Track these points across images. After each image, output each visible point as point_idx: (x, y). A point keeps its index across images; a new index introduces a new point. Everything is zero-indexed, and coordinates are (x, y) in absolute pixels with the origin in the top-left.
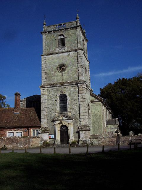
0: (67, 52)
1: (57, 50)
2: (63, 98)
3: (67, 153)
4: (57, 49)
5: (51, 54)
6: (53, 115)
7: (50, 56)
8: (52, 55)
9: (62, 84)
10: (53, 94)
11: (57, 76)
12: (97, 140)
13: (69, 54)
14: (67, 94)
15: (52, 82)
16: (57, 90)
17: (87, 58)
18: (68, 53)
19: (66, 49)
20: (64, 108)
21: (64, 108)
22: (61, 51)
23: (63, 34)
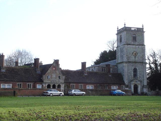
0: (137, 45)
1: (132, 43)
2: (135, 70)
3: (138, 90)
4: (132, 42)
5: (130, 44)
6: (130, 78)
7: (129, 46)
8: (119, 40)
9: (135, 62)
10: (131, 67)
11: (132, 58)
12: (150, 93)
13: (139, 47)
14: (137, 68)
15: (130, 61)
16: (133, 66)
17: (8, 80)
18: (138, 46)
19: (137, 43)
20: (135, 75)
21: (135, 75)
22: (134, 44)
23: (136, 34)
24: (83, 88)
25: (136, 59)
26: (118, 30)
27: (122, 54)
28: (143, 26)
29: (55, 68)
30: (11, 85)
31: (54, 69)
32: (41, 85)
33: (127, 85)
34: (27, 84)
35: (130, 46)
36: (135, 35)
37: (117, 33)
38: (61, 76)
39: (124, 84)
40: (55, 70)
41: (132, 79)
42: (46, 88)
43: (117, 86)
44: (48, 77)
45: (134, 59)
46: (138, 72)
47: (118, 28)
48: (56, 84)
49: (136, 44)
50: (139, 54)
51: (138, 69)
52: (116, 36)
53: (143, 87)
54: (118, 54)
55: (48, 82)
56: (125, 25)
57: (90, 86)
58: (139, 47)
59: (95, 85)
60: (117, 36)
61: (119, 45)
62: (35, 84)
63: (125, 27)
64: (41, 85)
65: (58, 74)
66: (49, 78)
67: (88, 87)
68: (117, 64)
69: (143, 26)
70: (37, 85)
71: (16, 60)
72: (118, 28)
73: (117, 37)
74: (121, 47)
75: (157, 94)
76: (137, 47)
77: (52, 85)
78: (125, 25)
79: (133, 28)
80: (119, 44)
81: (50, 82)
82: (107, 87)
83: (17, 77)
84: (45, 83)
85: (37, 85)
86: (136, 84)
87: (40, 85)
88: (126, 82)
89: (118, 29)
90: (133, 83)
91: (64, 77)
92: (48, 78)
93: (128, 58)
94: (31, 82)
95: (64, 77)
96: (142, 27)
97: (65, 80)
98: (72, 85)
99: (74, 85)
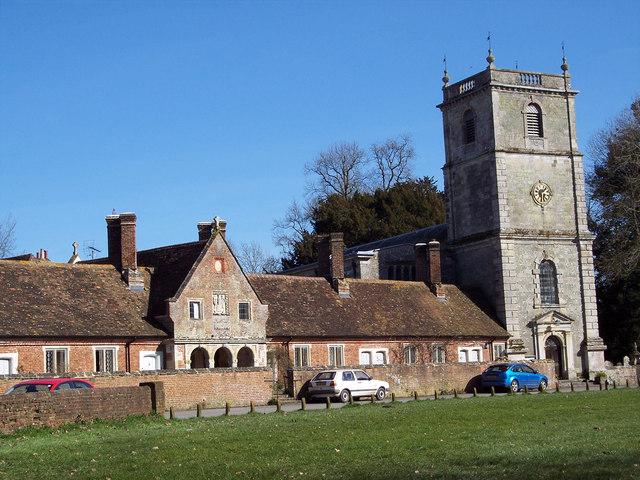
1: (529, 145)
7: (515, 156)
13: (555, 161)
14: (556, 262)
15: (522, 226)
18: (553, 158)
22: (535, 148)
24: (388, 360)
25: (549, 216)
26: (445, 89)
27: (482, 196)
29: (222, 260)
30: (15, 356)
31: (218, 265)
33: (517, 340)
34: (44, 349)
38: (252, 300)
40: (223, 270)
43: (480, 348)
44: (192, 310)
45: (537, 217)
48: (228, 346)
50: (557, 195)
52: (439, 113)
54: (455, 199)
55: (193, 335)
57: (374, 351)
58: (555, 161)
59: (394, 344)
61: (460, 155)
66: (196, 316)
68: (455, 243)
71: (609, 141)
72: (445, 80)
74: (472, 163)
79: (464, 82)
80: (459, 150)
81: (202, 334)
82: (440, 355)
83: (38, 311)
85: (142, 353)
89: (448, 85)
91: (264, 308)
92: (192, 315)
93: (516, 216)
94: (111, 339)
95: (264, 308)
97: (271, 323)
98: (297, 349)
99: (110, 353)
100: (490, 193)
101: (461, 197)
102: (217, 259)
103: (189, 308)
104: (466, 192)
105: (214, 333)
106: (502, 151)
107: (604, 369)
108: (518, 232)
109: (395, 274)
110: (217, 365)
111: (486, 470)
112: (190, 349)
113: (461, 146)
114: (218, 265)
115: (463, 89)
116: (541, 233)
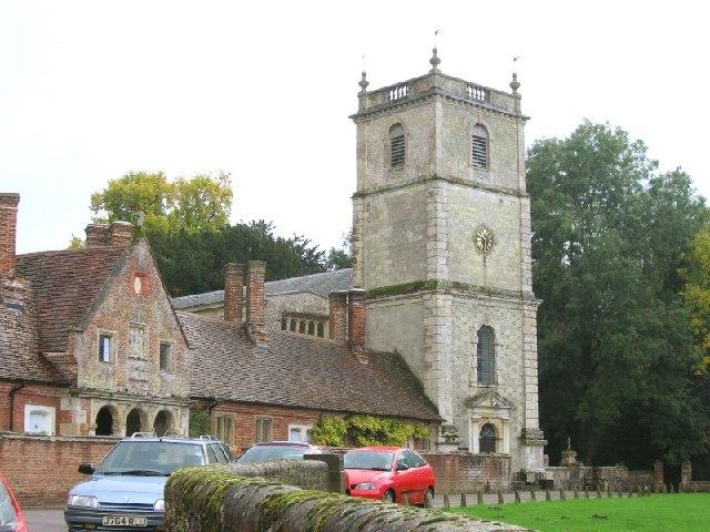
1: (471, 175)
7: (456, 188)
13: (501, 201)
14: (497, 328)
25: (490, 271)
26: (361, 96)
28: (515, 86)
29: (142, 276)
32: (51, 411)
35: (482, 198)
36: (483, 127)
37: (355, 110)
39: (435, 421)
40: (143, 292)
41: (473, 393)
42: (93, 433)
46: (498, 349)
47: (364, 84)
48: (145, 408)
49: (486, 182)
51: (498, 335)
52: (353, 127)
53: (523, 439)
56: (435, 61)
60: (360, 131)
62: (17, 398)
63: (433, 73)
64: (51, 411)
65: (160, 328)
66: (106, 358)
67: (296, 434)
69: (515, 86)
70: (29, 409)
72: (364, 84)
73: (358, 137)
75: (703, 484)
76: (493, 197)
77: (122, 414)
78: (435, 61)
84: (89, 395)
85: (29, 409)
86: (492, 422)
87: (44, 414)
88: (446, 409)
90: (478, 413)
92: (101, 358)
96: (510, 91)
100: (424, 232)
101: (378, 235)
102: (137, 275)
103: (98, 345)
104: (386, 231)
105: (129, 386)
106: (444, 179)
107: (542, 470)
108: (457, 285)
109: (316, 331)
110: (695, 477)
111: (140, 521)
112: (96, 407)
113: (382, 170)
114: (138, 284)
115: (394, 95)
116: (482, 290)
